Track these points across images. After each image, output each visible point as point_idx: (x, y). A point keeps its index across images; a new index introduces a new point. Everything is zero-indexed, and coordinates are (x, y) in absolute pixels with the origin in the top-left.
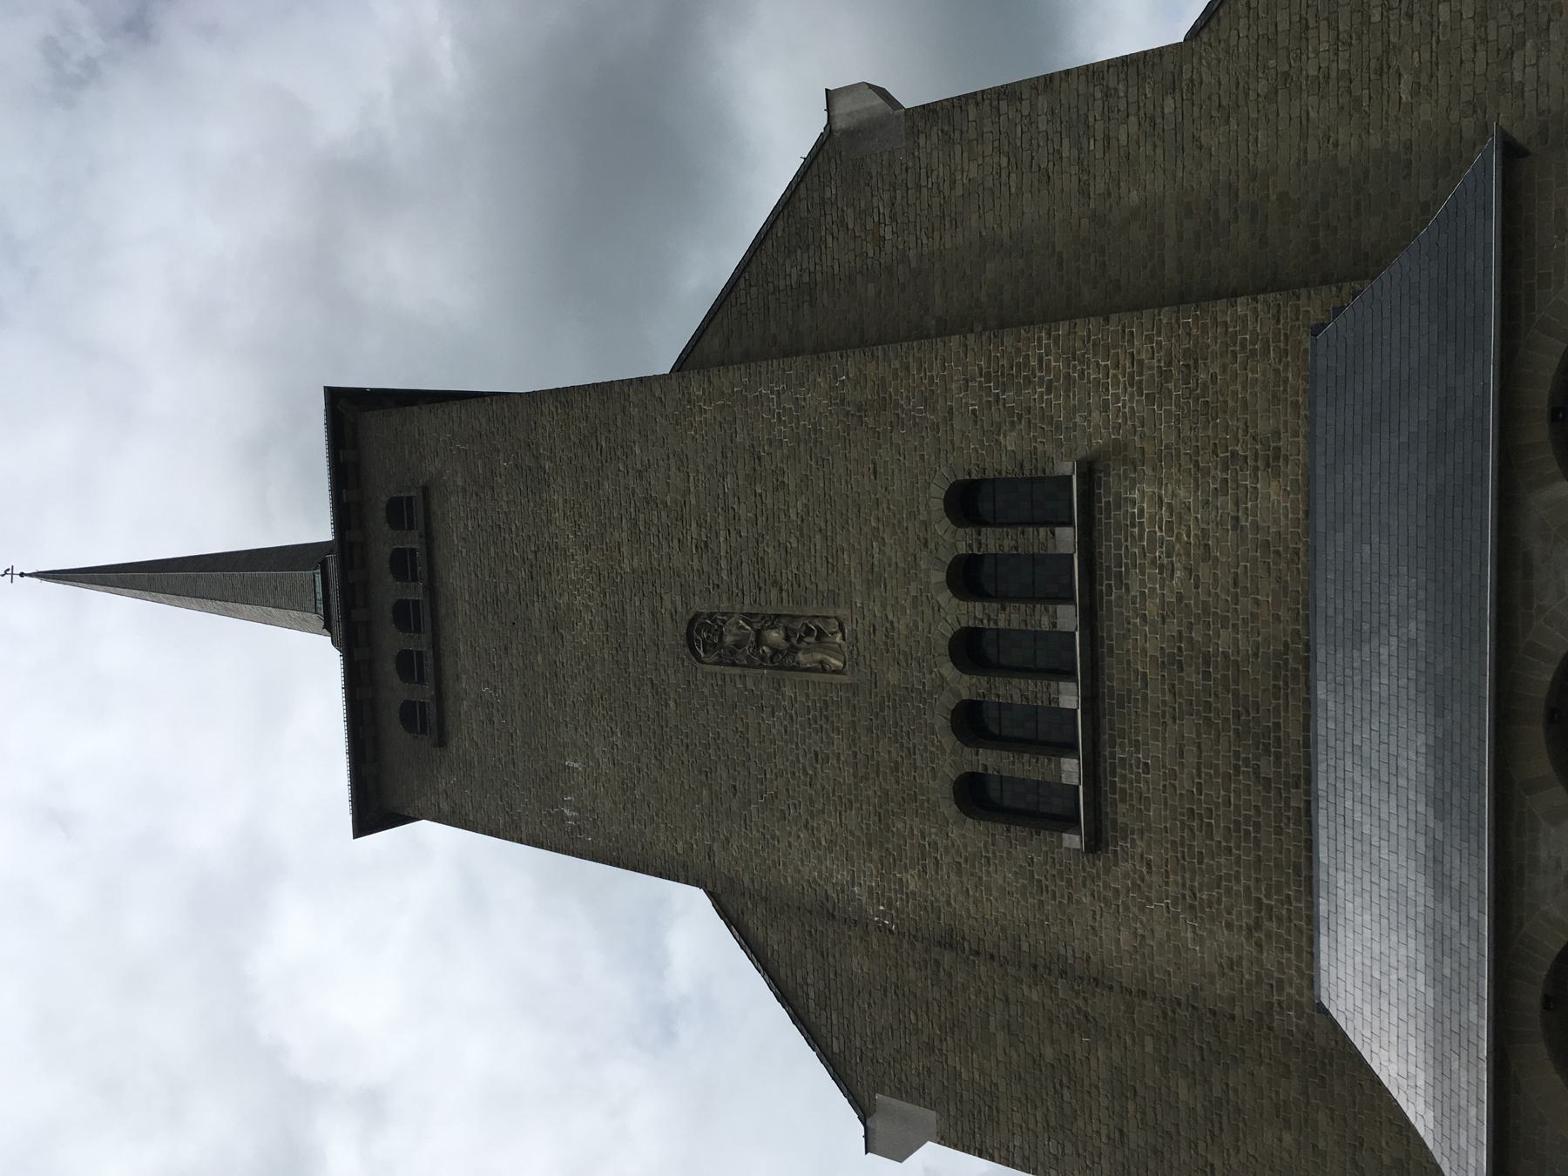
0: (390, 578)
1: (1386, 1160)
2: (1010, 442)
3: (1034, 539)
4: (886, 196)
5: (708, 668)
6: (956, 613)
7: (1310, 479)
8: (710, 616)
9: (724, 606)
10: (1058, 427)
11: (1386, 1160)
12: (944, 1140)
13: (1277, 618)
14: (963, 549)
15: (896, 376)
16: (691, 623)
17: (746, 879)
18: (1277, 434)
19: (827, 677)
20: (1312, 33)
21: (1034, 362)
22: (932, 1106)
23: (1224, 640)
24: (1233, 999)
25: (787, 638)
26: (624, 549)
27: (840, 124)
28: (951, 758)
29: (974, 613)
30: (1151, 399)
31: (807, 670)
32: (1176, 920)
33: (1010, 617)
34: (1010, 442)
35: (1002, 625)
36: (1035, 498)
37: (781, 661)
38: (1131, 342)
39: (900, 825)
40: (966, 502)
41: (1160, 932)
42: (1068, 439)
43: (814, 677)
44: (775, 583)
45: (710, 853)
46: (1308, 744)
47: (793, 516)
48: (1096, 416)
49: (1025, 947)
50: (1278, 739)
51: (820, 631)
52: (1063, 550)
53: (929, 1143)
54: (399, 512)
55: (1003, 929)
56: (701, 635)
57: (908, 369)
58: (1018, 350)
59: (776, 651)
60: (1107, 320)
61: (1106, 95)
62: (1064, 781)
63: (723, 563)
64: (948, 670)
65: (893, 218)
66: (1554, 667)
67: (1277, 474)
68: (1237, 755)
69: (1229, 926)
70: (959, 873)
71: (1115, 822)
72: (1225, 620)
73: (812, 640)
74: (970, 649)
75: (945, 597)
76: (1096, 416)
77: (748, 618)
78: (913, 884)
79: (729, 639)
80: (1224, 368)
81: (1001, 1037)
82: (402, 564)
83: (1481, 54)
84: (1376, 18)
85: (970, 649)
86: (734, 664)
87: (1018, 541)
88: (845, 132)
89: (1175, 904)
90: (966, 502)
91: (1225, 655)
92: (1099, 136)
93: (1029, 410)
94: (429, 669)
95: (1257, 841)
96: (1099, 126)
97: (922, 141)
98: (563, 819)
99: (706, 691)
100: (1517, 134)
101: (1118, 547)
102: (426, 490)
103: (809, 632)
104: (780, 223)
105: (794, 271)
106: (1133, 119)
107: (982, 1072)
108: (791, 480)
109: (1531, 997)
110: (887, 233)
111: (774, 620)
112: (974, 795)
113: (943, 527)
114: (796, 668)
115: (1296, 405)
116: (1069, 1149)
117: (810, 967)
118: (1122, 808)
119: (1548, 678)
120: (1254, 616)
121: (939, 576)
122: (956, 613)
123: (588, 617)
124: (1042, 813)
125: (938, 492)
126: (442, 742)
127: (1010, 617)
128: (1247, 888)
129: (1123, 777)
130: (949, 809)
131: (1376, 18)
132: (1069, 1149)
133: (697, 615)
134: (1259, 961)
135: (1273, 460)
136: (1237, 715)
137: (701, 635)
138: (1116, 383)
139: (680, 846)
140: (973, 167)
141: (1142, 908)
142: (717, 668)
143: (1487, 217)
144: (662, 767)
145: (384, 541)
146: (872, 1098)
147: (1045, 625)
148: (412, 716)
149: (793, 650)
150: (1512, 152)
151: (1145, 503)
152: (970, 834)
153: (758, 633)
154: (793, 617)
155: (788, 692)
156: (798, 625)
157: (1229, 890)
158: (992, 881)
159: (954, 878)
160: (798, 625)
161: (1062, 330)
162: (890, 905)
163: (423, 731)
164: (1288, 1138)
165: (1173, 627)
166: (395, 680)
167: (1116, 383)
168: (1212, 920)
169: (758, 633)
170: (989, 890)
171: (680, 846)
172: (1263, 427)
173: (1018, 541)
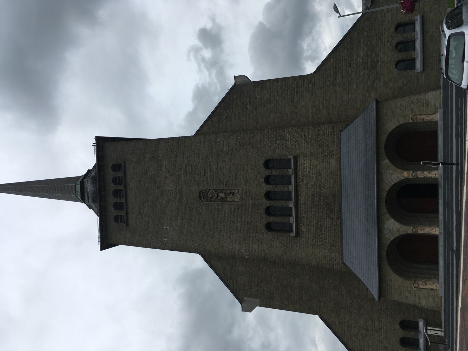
0: (112, 184)
1: (356, 294)
2: (278, 152)
3: (284, 172)
5: (204, 202)
6: (266, 188)
7: (340, 159)
8: (205, 190)
9: (209, 188)
11: (356, 294)
12: (260, 306)
13: (334, 186)
14: (268, 174)
15: (252, 137)
16: (200, 193)
17: (214, 251)
18: (333, 150)
19: (235, 203)
20: (338, 75)
21: (284, 135)
22: (258, 298)
24: (326, 264)
25: (225, 195)
26: (182, 176)
27: (236, 83)
28: (264, 219)
29: (270, 188)
30: (308, 143)
31: (230, 202)
32: (314, 249)
33: (278, 188)
34: (278, 152)
35: (276, 190)
36: (284, 163)
38: (304, 132)
42: (291, 151)
43: (232, 203)
46: (341, 211)
47: (227, 167)
48: (297, 147)
49: (281, 258)
50: (334, 211)
51: (234, 193)
52: (290, 174)
53: (257, 307)
54: (116, 168)
56: (203, 195)
58: (280, 133)
59: (222, 198)
60: (299, 128)
61: (297, 83)
62: (419, 177)
63: (209, 178)
64: (264, 200)
65: (250, 104)
66: (386, 193)
67: (333, 158)
68: (326, 214)
70: (266, 244)
71: (301, 230)
73: (231, 195)
74: (268, 195)
76: (297, 147)
77: (215, 190)
79: (210, 196)
80: (323, 138)
82: (116, 181)
83: (369, 82)
84: (350, 73)
85: (268, 195)
86: (211, 201)
87: (277, 171)
89: (314, 245)
90: (267, 164)
91: (324, 194)
92: (296, 90)
93: (282, 145)
94: (125, 207)
95: (330, 231)
97: (257, 88)
98: (163, 241)
100: (379, 100)
101: (302, 173)
102: (124, 162)
103: (230, 193)
104: (223, 103)
106: (302, 88)
109: (384, 253)
110: (249, 107)
111: (222, 191)
112: (269, 227)
113: (263, 170)
114: (227, 201)
115: (337, 145)
116: (290, 303)
118: (303, 227)
119: (385, 194)
120: (330, 187)
121: (262, 180)
122: (266, 188)
123: (171, 192)
124: (286, 229)
125: (262, 162)
126: (127, 225)
127: (278, 188)
128: (329, 241)
129: (303, 221)
131: (350, 73)
132: (290, 303)
133: (202, 190)
134: (331, 256)
135: (333, 155)
136: (326, 206)
137: (203, 195)
138: (301, 140)
139: (196, 245)
141: (307, 248)
142: (207, 202)
143: (373, 113)
145: (110, 175)
147: (286, 189)
148: (118, 219)
149: (226, 197)
150: (377, 102)
151: (304, 163)
153: (218, 194)
154: (226, 190)
155: (225, 207)
156: (228, 192)
157: (325, 242)
158: (273, 246)
159: (265, 245)
160: (228, 192)
161: (290, 129)
162: (250, 253)
163: (121, 222)
164: (336, 292)
166: (113, 210)
167: (301, 140)
169: (218, 194)
170: (273, 247)
171: (196, 245)
173: (277, 171)
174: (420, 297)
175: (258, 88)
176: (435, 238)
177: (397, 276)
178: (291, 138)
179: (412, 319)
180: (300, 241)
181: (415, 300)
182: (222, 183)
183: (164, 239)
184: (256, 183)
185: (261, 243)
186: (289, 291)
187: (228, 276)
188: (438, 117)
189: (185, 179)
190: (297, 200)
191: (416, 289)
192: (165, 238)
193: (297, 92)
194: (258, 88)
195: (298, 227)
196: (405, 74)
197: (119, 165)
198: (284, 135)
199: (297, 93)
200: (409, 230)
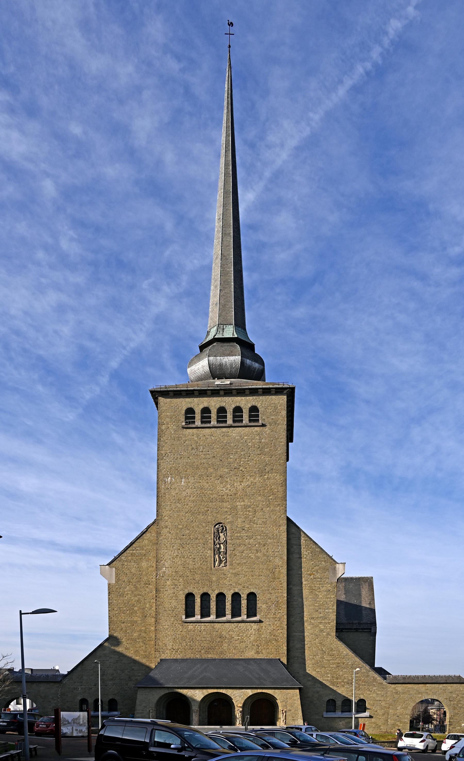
1: (133, 668)
4: (320, 577)
10: (266, 616)
21: (279, 611)
23: (226, 645)
26: (242, 503)
30: (270, 633)
36: (252, 612)
37: (217, 551)
39: (181, 580)
40: (252, 597)
41: (169, 633)
43: (213, 559)
44: (234, 549)
45: (166, 527)
47: (250, 555)
55: (163, 603)
57: (281, 584)
61: (329, 623)
64: (217, 592)
69: (173, 645)
72: (229, 645)
75: (232, 592)
78: (168, 583)
81: (137, 598)
88: (335, 567)
96: (324, 621)
97: (329, 585)
99: (207, 528)
105: (307, 553)
107: (127, 594)
108: (259, 554)
112: (190, 597)
113: (247, 592)
116: (117, 612)
117: (141, 551)
121: (237, 591)
124: (189, 613)
130: (187, 592)
137: (220, 528)
140: (322, 596)
144: (186, 513)
146: (113, 567)
152: (183, 597)
155: (209, 552)
165: (227, 636)
168: (173, 642)
170: (170, 600)
172: (264, 651)
174: (143, 713)
175: (330, 587)
176: (231, 722)
177: (157, 699)
178: (276, 618)
179: (118, 707)
180: (179, 624)
181: (139, 710)
182: (234, 549)
183: (169, 478)
184: (234, 584)
185: (174, 588)
186: (128, 612)
187: (134, 552)
188: (281, 724)
189: (239, 507)
190: (302, 757)
191: (148, 710)
192: (171, 480)
193: (321, 623)
194: (330, 587)
195: (127, 549)
196: (324, 705)
197: (258, 416)
198: (279, 611)
199: (319, 623)
200: (238, 714)
